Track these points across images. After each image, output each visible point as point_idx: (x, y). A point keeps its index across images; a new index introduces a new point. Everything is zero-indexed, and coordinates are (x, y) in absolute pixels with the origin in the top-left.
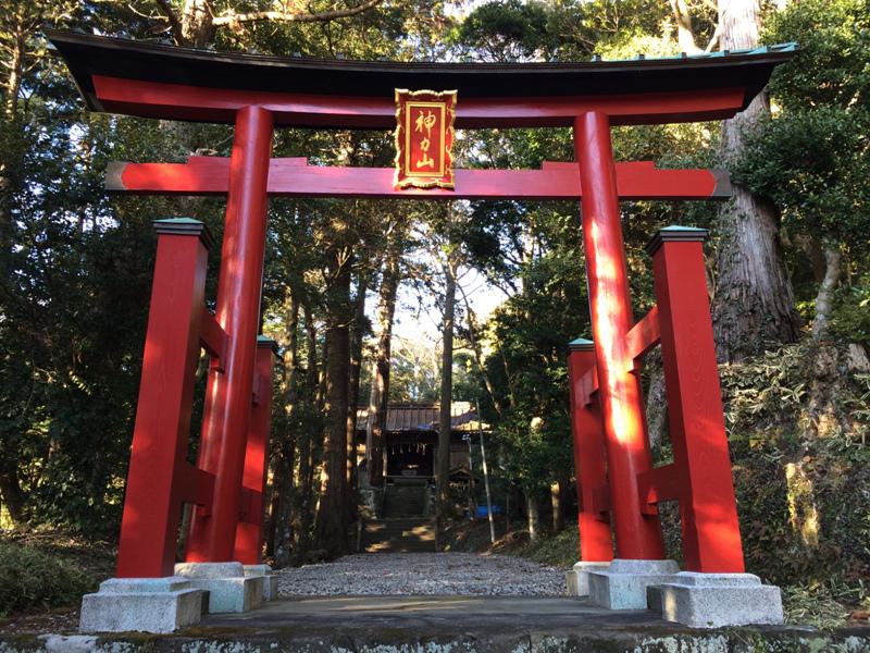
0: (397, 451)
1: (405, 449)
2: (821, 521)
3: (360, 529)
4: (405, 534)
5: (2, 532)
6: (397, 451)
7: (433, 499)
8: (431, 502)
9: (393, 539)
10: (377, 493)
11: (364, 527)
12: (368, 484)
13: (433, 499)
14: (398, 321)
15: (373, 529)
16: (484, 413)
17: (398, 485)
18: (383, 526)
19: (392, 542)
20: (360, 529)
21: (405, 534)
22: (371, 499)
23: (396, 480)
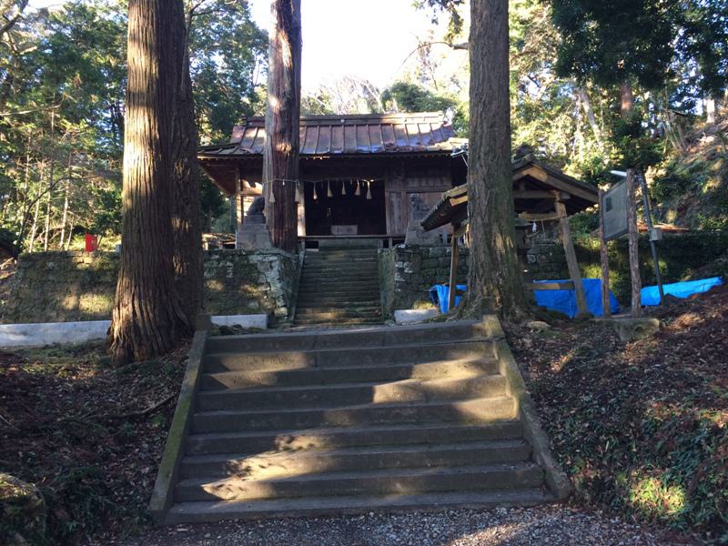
0: (322, 193)
1: (336, 188)
2: (441, 355)
3: (191, 378)
4: (384, 392)
5: (721, 356)
6: (322, 193)
7: (401, 270)
8: (397, 277)
9: (340, 416)
10: (285, 261)
11: (211, 364)
12: (268, 245)
13: (401, 270)
14: (391, 78)
15: (259, 370)
16: (673, 83)
17: (329, 249)
18: (295, 361)
19: (341, 440)
20: (191, 378)
21: (384, 392)
22: (273, 275)
23: (322, 242)
